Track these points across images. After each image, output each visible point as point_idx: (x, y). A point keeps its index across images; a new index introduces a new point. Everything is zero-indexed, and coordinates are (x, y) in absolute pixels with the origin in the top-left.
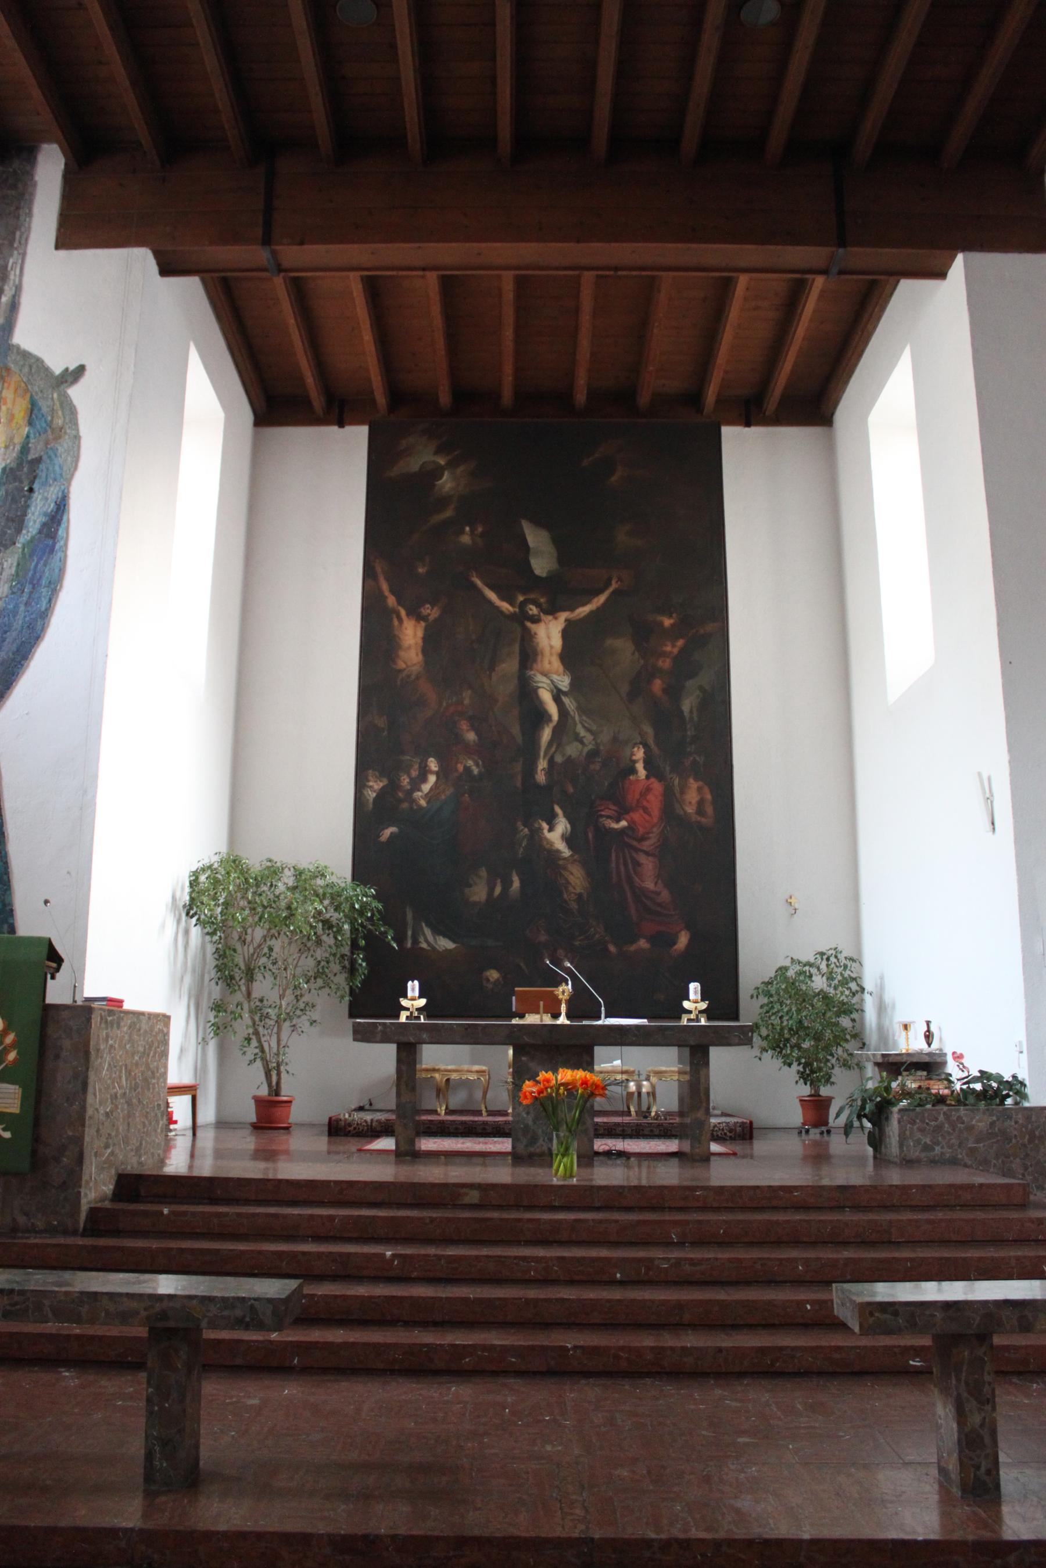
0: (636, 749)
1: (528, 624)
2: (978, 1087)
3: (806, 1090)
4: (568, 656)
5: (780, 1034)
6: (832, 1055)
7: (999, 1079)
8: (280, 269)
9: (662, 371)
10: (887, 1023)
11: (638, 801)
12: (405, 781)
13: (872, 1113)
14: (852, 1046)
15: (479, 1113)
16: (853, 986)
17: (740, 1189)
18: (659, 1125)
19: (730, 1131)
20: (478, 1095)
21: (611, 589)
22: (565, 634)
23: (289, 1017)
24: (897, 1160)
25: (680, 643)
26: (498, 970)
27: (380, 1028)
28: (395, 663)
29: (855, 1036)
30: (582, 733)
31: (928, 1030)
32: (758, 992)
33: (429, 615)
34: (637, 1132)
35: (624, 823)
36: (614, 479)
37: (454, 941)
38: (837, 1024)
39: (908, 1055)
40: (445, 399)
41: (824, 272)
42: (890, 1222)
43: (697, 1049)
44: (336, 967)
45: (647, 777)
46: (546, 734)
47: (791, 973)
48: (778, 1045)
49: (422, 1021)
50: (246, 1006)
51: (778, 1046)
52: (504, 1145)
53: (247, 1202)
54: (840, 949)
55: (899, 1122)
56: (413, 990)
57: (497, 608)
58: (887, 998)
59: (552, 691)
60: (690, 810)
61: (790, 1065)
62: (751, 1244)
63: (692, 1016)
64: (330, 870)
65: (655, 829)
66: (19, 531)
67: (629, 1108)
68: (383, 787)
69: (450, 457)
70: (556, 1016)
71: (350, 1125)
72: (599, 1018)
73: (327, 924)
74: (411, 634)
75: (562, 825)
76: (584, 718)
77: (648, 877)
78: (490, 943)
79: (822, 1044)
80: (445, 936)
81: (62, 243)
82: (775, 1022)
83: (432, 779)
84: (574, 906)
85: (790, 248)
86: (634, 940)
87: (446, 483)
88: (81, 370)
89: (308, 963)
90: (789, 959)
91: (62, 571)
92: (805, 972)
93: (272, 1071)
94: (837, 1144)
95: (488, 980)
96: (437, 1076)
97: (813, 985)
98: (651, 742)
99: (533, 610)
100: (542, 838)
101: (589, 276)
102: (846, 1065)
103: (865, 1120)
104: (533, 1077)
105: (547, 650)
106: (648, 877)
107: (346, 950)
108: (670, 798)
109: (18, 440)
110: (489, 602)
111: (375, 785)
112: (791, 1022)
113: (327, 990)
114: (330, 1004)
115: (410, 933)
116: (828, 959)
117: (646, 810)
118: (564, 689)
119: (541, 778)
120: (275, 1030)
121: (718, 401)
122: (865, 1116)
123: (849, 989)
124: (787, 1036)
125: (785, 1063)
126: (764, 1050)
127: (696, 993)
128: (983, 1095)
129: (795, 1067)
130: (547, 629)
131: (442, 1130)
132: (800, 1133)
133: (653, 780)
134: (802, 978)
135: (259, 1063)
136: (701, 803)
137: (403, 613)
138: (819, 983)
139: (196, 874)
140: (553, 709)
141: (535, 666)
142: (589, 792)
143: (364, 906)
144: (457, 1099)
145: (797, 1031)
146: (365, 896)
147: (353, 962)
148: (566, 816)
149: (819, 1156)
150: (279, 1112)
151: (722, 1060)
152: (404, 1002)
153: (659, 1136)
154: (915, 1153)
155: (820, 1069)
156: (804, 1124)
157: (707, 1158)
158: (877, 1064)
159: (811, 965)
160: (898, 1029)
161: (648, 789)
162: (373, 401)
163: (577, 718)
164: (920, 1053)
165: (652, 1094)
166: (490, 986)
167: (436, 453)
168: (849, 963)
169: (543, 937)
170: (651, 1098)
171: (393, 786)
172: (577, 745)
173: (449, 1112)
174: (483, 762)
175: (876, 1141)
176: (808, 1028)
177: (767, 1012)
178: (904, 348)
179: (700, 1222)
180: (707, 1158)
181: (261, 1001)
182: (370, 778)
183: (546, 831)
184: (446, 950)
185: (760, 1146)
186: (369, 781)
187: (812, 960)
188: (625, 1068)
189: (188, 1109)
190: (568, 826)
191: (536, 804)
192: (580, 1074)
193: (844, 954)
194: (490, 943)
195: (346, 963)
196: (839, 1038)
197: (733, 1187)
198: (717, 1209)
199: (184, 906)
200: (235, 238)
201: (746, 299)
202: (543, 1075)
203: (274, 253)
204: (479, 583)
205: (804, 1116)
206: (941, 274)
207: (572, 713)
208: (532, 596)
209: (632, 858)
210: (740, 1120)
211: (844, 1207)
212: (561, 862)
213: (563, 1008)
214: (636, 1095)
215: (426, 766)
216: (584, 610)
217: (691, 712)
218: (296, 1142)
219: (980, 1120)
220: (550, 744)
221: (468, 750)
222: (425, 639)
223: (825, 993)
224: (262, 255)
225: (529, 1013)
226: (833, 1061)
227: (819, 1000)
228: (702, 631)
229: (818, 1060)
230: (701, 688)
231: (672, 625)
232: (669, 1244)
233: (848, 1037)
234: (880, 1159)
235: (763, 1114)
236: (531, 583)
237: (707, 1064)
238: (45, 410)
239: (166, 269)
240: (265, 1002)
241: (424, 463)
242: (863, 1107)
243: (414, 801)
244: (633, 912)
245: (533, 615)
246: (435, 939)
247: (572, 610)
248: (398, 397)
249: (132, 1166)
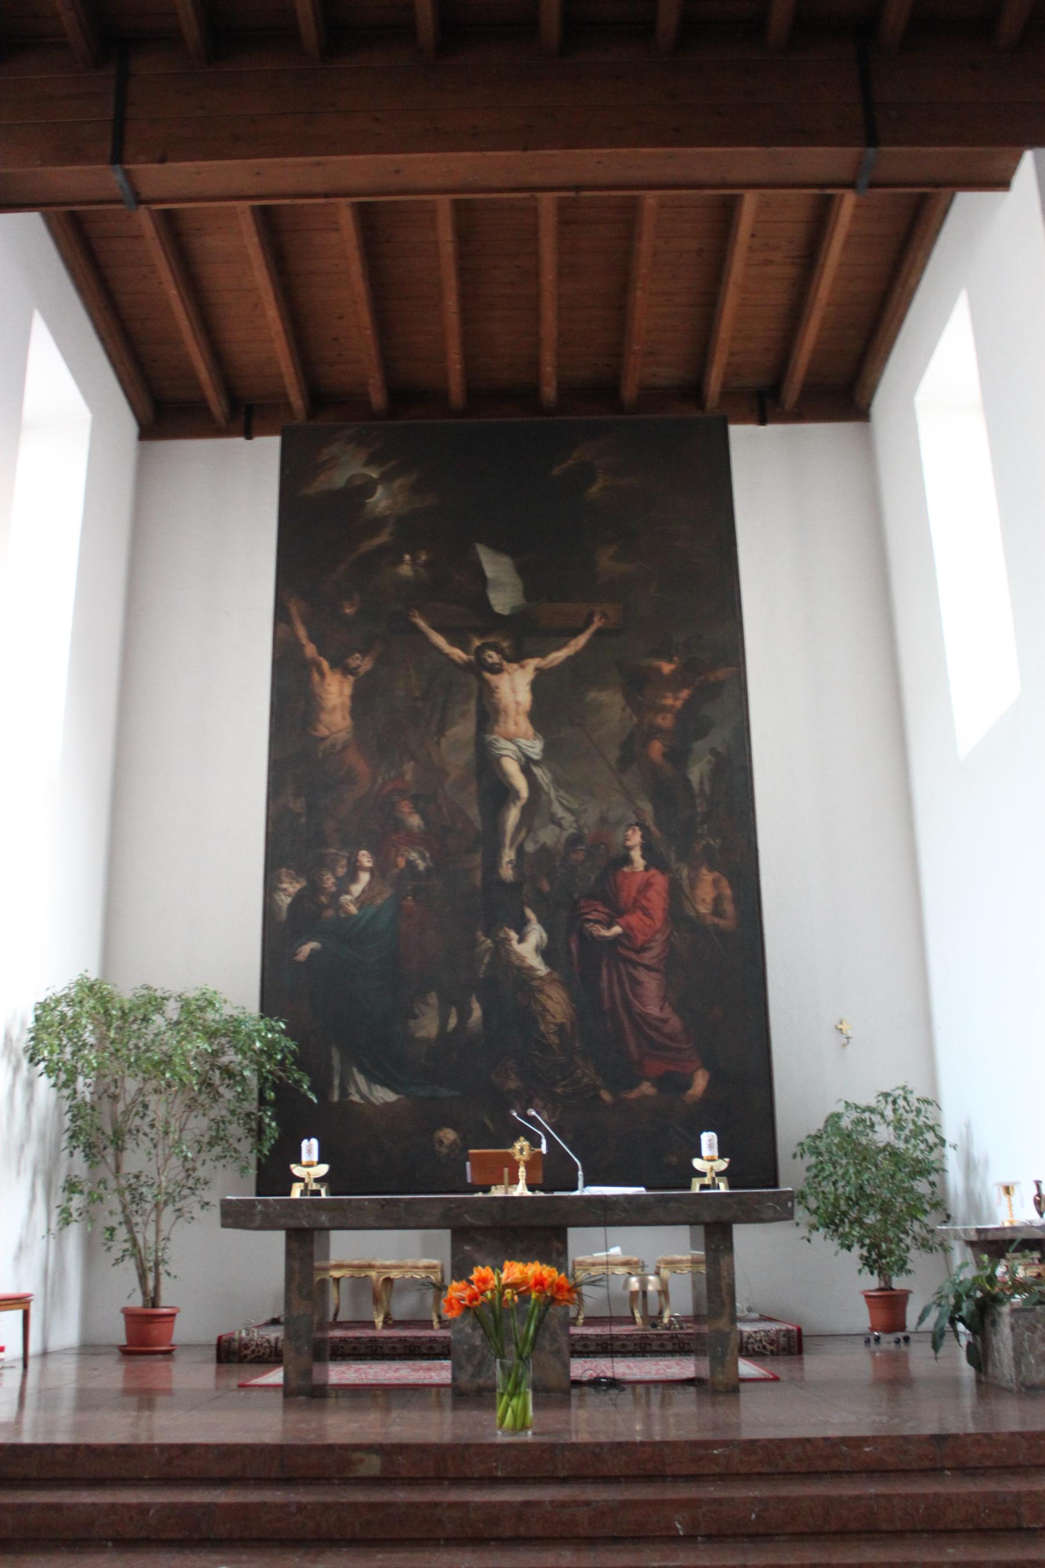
0: (630, 832)
1: (487, 675)
3: (873, 1282)
4: (540, 716)
5: (833, 1205)
6: (906, 1232)
9: (650, 360)
10: (977, 1186)
11: (635, 900)
12: (329, 881)
13: (972, 1315)
14: (931, 1219)
15: (428, 1324)
16: (930, 1137)
17: (781, 1443)
18: (673, 1337)
19: (771, 1344)
21: (593, 628)
22: (536, 687)
23: (170, 1198)
24: (1013, 1386)
25: (685, 694)
26: (454, 1128)
27: (259, 1207)
28: (315, 730)
30: (560, 812)
31: (1039, 1195)
32: (802, 1149)
33: (359, 666)
34: (641, 1347)
35: (617, 929)
36: (594, 489)
37: (396, 1092)
38: (911, 1190)
39: (1013, 1229)
40: (378, 398)
41: (851, 185)
42: (1018, 1494)
44: (236, 1130)
45: (647, 868)
46: (513, 816)
47: (846, 1123)
48: (832, 1220)
49: (324, 1196)
50: (112, 1184)
51: (833, 1222)
52: (440, 1372)
54: (910, 1087)
55: (1012, 1328)
56: (309, 1151)
57: (447, 655)
58: (977, 1153)
59: (519, 760)
60: (704, 909)
61: (849, 1248)
62: (799, 1536)
63: (707, 1181)
64: (223, 997)
65: (658, 937)
67: (633, 1313)
68: (301, 889)
69: (383, 469)
70: (514, 1181)
71: (246, 1346)
72: (576, 1189)
74: (336, 692)
75: (536, 934)
76: (562, 793)
77: (652, 998)
78: (444, 1092)
79: (892, 1218)
80: (384, 1084)
82: (827, 1190)
83: (365, 877)
84: (554, 1039)
85: (803, 149)
86: (634, 1084)
87: (380, 501)
89: (199, 1124)
90: (843, 1104)
92: (864, 1121)
94: (920, 1358)
95: (441, 1142)
96: (373, 1274)
97: (876, 1137)
98: (650, 822)
99: (493, 657)
100: (509, 952)
101: (547, 201)
102: (925, 1245)
103: (961, 1327)
105: (512, 707)
106: (652, 998)
108: (676, 893)
111: (291, 887)
112: (848, 1189)
115: (336, 1082)
116: (894, 1102)
118: (536, 757)
119: (507, 872)
120: (153, 1216)
122: (962, 1320)
123: (925, 1141)
124: (844, 1208)
125: (842, 1245)
127: (711, 1146)
129: (856, 1250)
130: (512, 681)
132: (868, 1341)
133: (653, 871)
134: (860, 1128)
135: (130, 1263)
136: (718, 900)
137: (325, 665)
138: (884, 1135)
140: (521, 783)
141: (496, 729)
142: (575, 888)
143: (271, 1045)
145: (858, 1199)
147: (260, 1121)
148: (542, 921)
149: (895, 1380)
150: (156, 1330)
151: (745, 1237)
152: (297, 1170)
155: (891, 1252)
156: (873, 1329)
157: (733, 1387)
158: (970, 1244)
159: (872, 1110)
160: (995, 1193)
161: (648, 885)
162: (288, 405)
163: (553, 794)
164: (1030, 1226)
165: (664, 1292)
166: (444, 1150)
167: (367, 463)
168: (922, 1106)
169: (513, 1084)
170: (663, 1299)
172: (552, 829)
173: (388, 1323)
174: (431, 854)
175: (980, 1357)
176: (872, 1196)
177: (816, 1176)
178: (955, 299)
179: (718, 1501)
180: (733, 1387)
181: (137, 1177)
182: (284, 878)
183: (514, 943)
184: (386, 1104)
185: (814, 1364)
186: (281, 883)
187: (873, 1104)
188: (627, 1257)
190: (544, 935)
191: (502, 908)
192: (534, 1269)
193: (917, 1094)
194: (444, 1092)
195: (254, 1125)
196: (914, 1211)
197: (770, 1441)
198: (747, 1477)
199: (26, 1050)
200: (76, 155)
201: (751, 249)
203: (128, 175)
204: (422, 624)
205: (872, 1318)
206: (1003, 183)
207: (546, 788)
208: (491, 640)
209: (629, 974)
210: (784, 1327)
211: (943, 1469)
212: (535, 983)
213: (522, 1172)
214: (641, 1294)
215: (357, 861)
216: (559, 656)
217: (701, 782)
220: (518, 828)
221: (412, 839)
222: (354, 697)
223: (892, 1147)
224: (113, 178)
226: (908, 1241)
227: (885, 1159)
228: (712, 678)
229: (888, 1240)
230: (714, 752)
231: (673, 672)
233: (927, 1207)
234: (986, 1384)
235: (933, 1154)
236: (490, 622)
237: (730, 1249)
240: (143, 1179)
241: (352, 476)
242: (957, 1307)
243: (339, 907)
244: (633, 1046)
245: (493, 664)
246: (370, 1089)
247: (543, 655)
248: (321, 399)
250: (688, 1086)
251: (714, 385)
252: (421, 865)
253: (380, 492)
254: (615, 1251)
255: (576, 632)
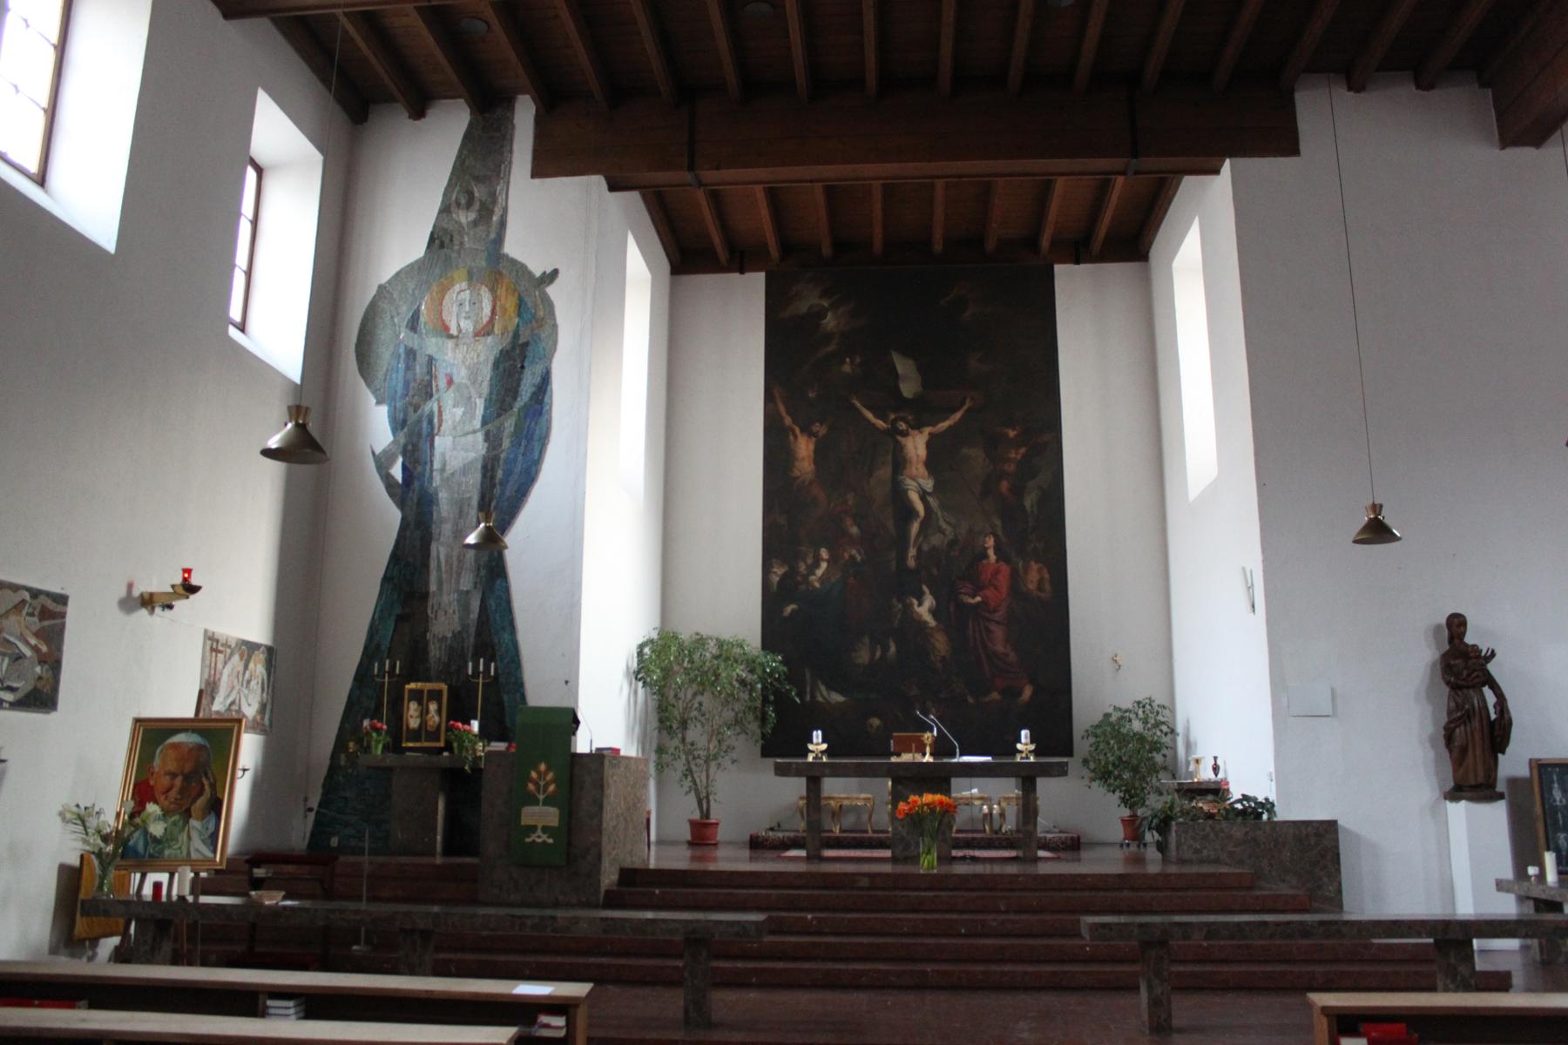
2: (1239, 806)
3: (1126, 813)
4: (931, 464)
7: (1254, 799)
8: (701, 184)
12: (802, 568)
20: (865, 817)
22: (929, 445)
23: (715, 757)
25: (1023, 450)
26: (879, 717)
29: (1165, 768)
30: (944, 526)
32: (1088, 734)
34: (989, 844)
35: (978, 599)
40: (826, 250)
41: (1123, 173)
43: (1028, 778)
44: (750, 717)
46: (915, 527)
47: (1113, 719)
48: (1103, 776)
53: (710, 886)
58: (1192, 739)
60: (1032, 586)
66: (515, 399)
70: (924, 755)
72: (954, 755)
73: (743, 682)
74: (804, 448)
75: (929, 601)
80: (835, 690)
81: (538, 172)
83: (824, 565)
84: (939, 665)
87: (830, 322)
88: (555, 273)
89: (729, 715)
91: (548, 429)
93: (703, 801)
99: (903, 426)
100: (913, 612)
104: (905, 800)
105: (914, 459)
107: (758, 703)
108: (1014, 574)
109: (511, 328)
110: (868, 421)
111: (779, 571)
113: (743, 736)
114: (746, 745)
117: (996, 588)
119: (911, 563)
121: (1053, 243)
126: (1093, 780)
128: (1243, 812)
131: (838, 843)
136: (1041, 581)
137: (797, 430)
138: (1137, 726)
139: (641, 647)
142: (952, 572)
143: (773, 670)
144: (849, 821)
146: (774, 662)
151: (1046, 788)
152: (811, 747)
153: (1005, 848)
154: (1188, 855)
161: (998, 571)
164: (1209, 782)
165: (1002, 815)
169: (914, 692)
171: (793, 571)
173: (842, 831)
180: (1037, 859)
185: (1084, 854)
189: (652, 827)
191: (907, 585)
192: (938, 797)
196: (1154, 769)
202: (912, 798)
204: (858, 405)
206: (1216, 172)
213: (928, 749)
218: (721, 852)
219: (1238, 831)
222: (816, 451)
224: (688, 177)
225: (1353, 69)
232: (998, 912)
234: (1165, 860)
236: (901, 403)
237: (1034, 790)
238: (530, 305)
239: (613, 187)
243: (809, 583)
248: (788, 248)
249: (628, 864)
250: (1020, 693)
251: (1045, 243)
252: (859, 558)
253: (829, 315)
254: (975, 791)
255: (954, 410)
